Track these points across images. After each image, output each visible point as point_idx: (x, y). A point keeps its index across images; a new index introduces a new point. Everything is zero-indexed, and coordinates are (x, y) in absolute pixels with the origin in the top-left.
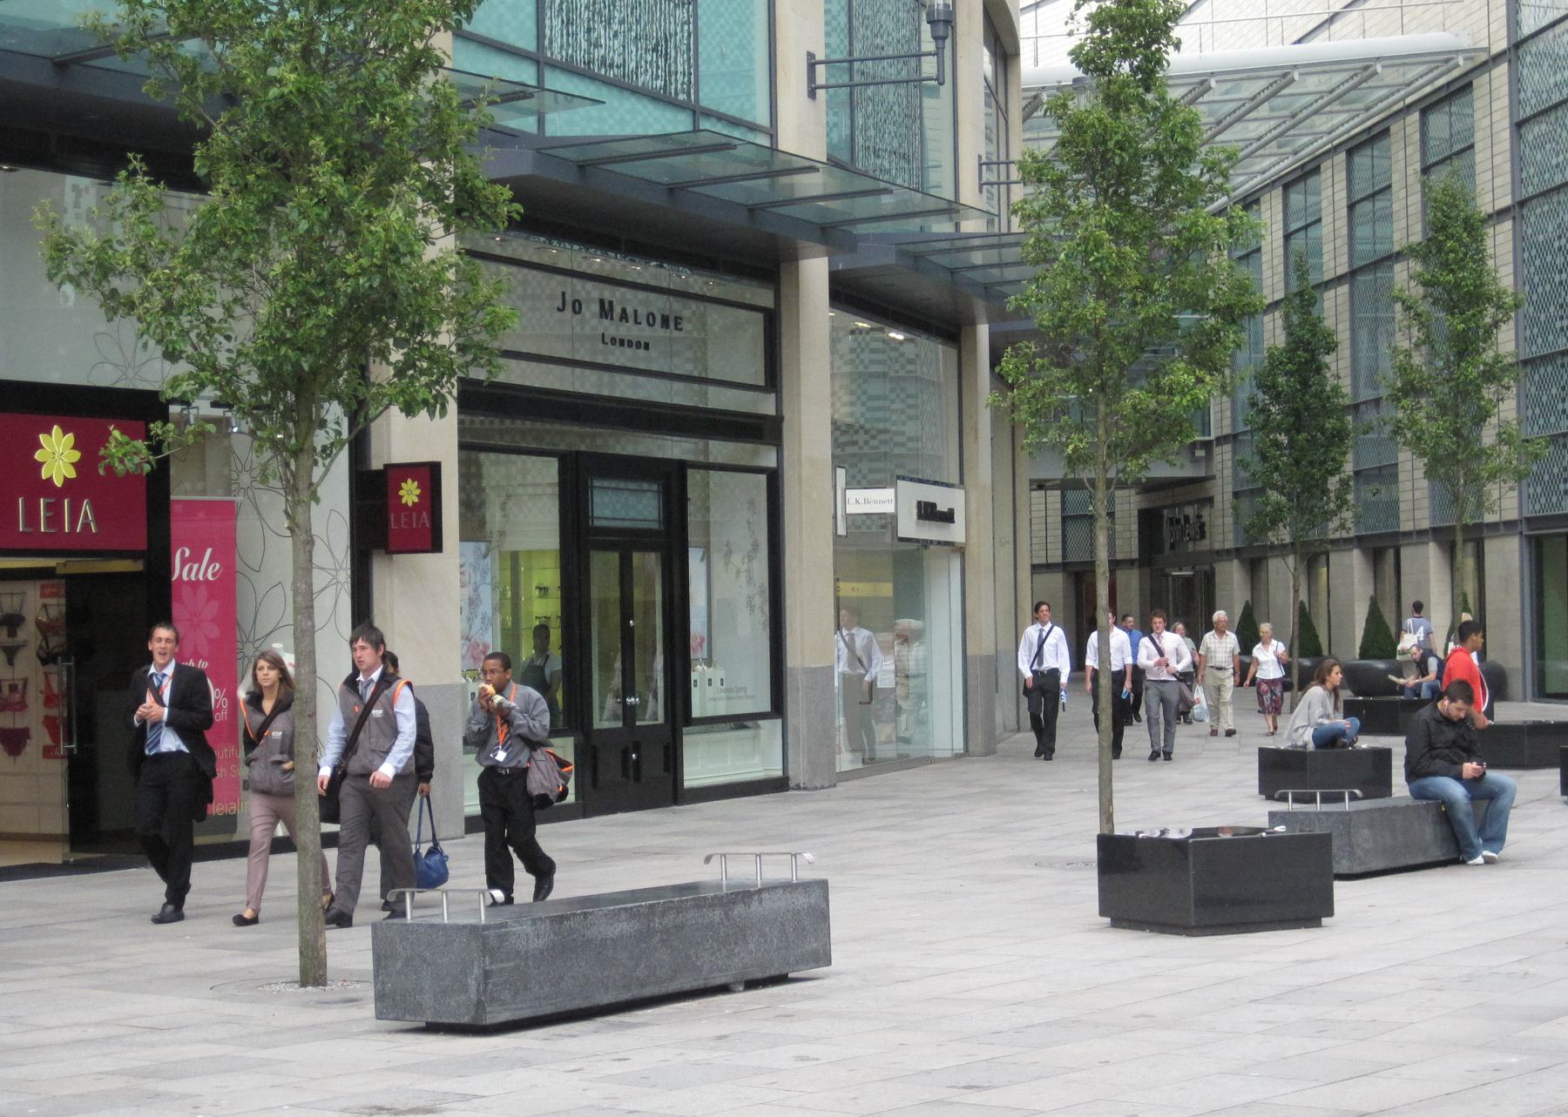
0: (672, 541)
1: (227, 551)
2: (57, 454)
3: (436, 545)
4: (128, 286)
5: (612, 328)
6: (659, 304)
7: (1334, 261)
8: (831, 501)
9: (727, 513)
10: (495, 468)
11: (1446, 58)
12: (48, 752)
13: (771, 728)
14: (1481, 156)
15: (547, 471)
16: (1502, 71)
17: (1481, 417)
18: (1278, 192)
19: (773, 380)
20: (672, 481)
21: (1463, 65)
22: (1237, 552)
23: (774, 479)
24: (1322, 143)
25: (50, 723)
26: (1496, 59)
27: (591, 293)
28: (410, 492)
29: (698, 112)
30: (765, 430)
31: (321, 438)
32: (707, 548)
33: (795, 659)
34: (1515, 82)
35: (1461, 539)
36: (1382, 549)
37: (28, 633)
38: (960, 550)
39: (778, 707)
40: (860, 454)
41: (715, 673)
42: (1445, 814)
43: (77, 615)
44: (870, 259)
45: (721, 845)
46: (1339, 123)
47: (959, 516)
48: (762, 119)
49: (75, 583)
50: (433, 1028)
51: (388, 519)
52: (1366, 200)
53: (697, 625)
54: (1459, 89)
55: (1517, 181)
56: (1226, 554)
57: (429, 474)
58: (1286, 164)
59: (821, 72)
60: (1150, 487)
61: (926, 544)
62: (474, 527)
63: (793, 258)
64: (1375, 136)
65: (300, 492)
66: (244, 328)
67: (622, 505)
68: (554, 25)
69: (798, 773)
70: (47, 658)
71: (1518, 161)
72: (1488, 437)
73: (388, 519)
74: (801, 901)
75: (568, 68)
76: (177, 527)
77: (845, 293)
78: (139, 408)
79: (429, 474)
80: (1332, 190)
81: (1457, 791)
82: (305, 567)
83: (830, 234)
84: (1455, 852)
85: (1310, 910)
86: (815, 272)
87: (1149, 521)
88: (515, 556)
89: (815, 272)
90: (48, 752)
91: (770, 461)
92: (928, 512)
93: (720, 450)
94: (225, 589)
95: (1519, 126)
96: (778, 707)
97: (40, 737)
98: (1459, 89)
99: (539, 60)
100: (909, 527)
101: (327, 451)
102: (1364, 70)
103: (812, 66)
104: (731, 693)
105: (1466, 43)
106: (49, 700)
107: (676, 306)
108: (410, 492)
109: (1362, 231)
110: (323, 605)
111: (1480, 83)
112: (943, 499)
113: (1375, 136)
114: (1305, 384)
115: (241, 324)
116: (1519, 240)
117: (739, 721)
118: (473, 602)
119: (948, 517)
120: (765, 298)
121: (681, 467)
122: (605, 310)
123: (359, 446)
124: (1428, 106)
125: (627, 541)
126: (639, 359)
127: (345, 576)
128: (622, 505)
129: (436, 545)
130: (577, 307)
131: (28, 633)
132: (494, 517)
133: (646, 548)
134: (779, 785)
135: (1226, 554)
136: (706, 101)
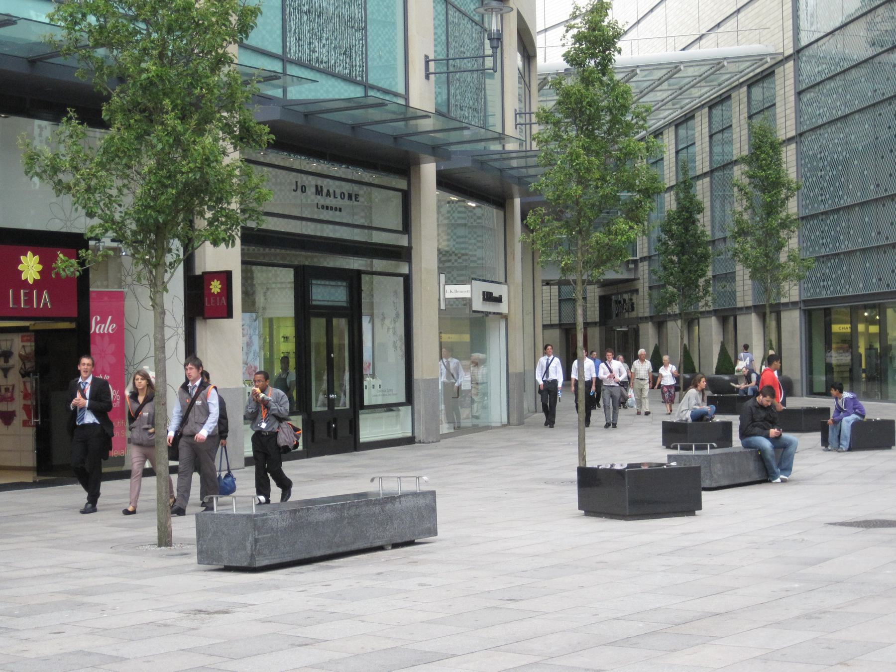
1: (119, 317)
2: (30, 267)
3: (229, 315)
4: (67, 178)
6: (347, 187)
7: (702, 165)
9: (383, 297)
10: (261, 274)
11: (761, 58)
13: (406, 411)
14: (779, 109)
15: (288, 275)
16: (790, 65)
19: (407, 227)
20: (353, 280)
21: (770, 62)
23: (408, 280)
24: (696, 103)
25: (26, 408)
26: (787, 58)
27: (311, 181)
28: (216, 287)
29: (367, 86)
30: (403, 254)
31: (169, 258)
34: (797, 71)
35: (769, 311)
36: (727, 317)
37: (15, 361)
38: (505, 317)
39: (410, 399)
40: (453, 266)
41: (377, 382)
42: (760, 456)
43: (40, 352)
44: (459, 164)
47: (505, 299)
48: (401, 90)
50: (228, 569)
54: (768, 75)
55: (798, 123)
58: (677, 114)
59: (432, 66)
60: (605, 284)
61: (487, 314)
62: (249, 305)
63: (417, 163)
64: (724, 99)
65: (158, 287)
66: (128, 200)
68: (292, 40)
69: (420, 435)
71: (799, 112)
73: (204, 301)
74: (421, 502)
76: (93, 305)
77: (445, 182)
79: (226, 277)
80: (701, 128)
81: (766, 444)
82: (160, 326)
83: (437, 151)
85: (688, 505)
86: (429, 171)
87: (604, 301)
88: (271, 320)
89: (429, 171)
90: (25, 424)
91: (405, 271)
92: (488, 297)
93: (379, 264)
94: (118, 338)
95: (799, 94)
97: (21, 416)
98: (768, 75)
99: (284, 59)
100: (478, 305)
102: (717, 64)
103: (427, 62)
105: (771, 50)
106: (26, 396)
107: (355, 188)
108: (216, 287)
109: (717, 149)
110: (170, 346)
111: (779, 71)
113: (724, 99)
114: (686, 229)
115: (127, 198)
117: (389, 407)
118: (249, 345)
119: (499, 300)
120: (402, 184)
121: (359, 273)
122: (319, 191)
124: (751, 84)
125: (330, 312)
127: (181, 331)
129: (229, 315)
130: (304, 189)
131: (15, 361)
132: (260, 299)
134: (410, 441)
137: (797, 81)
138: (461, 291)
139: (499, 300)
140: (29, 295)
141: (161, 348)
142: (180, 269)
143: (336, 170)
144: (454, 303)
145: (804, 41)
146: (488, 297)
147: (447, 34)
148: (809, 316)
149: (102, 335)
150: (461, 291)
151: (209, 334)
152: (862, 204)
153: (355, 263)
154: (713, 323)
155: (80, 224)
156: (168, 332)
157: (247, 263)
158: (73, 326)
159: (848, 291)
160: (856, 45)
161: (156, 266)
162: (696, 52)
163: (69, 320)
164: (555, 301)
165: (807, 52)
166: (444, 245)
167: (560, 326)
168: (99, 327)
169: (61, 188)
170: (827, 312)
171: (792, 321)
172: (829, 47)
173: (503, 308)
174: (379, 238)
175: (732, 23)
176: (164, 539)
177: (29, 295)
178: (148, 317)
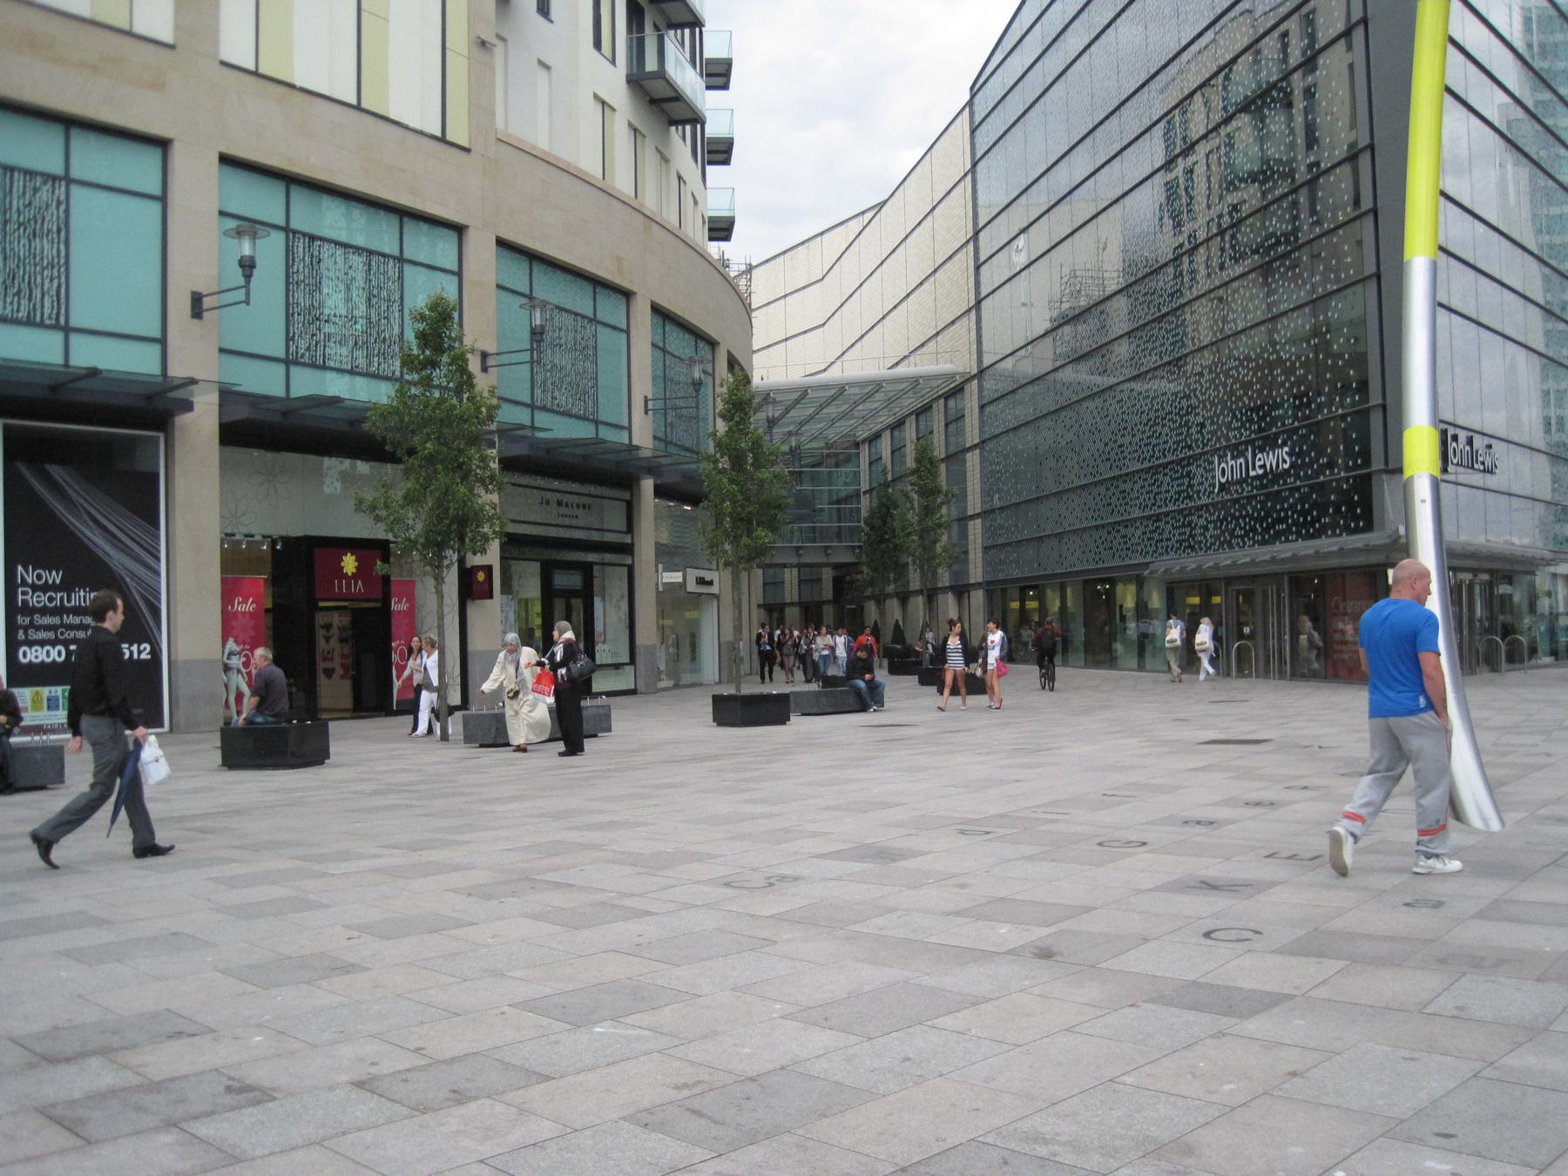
0: (587, 594)
1: (411, 599)
2: (349, 563)
3: (491, 597)
4: (383, 513)
5: (563, 510)
6: (583, 500)
7: (939, 452)
8: (657, 577)
9: (614, 583)
10: (517, 567)
11: (952, 376)
12: (342, 677)
13: (629, 669)
14: (967, 420)
15: (535, 567)
16: (975, 382)
17: (935, 542)
18: (888, 432)
19: (630, 528)
20: (586, 569)
21: (959, 380)
22: (951, 588)
23: (631, 569)
24: (906, 411)
25: (343, 665)
26: (973, 377)
27: (554, 497)
28: (481, 576)
29: (597, 422)
30: (628, 549)
31: (446, 562)
32: (604, 599)
33: (639, 641)
34: (980, 387)
35: (961, 591)
36: (904, 599)
37: (335, 631)
38: (716, 597)
39: (632, 661)
40: (668, 555)
41: (606, 647)
42: (858, 692)
43: (354, 624)
44: (671, 478)
45: (770, 816)
46: (910, 403)
47: (716, 583)
48: (626, 423)
49: (355, 612)
50: (482, 746)
51: (472, 588)
52: (955, 420)
53: (599, 627)
54: (958, 391)
55: (981, 432)
56: (945, 590)
57: (488, 569)
58: (891, 420)
59: (650, 405)
60: (836, 566)
61: (700, 594)
62: (507, 587)
63: (638, 480)
64: (927, 408)
65: (439, 580)
66: (419, 527)
67: (562, 580)
68: (538, 392)
69: (641, 687)
70: (343, 640)
71: (982, 424)
72: (939, 549)
73: (472, 588)
74: (601, 711)
75: (544, 409)
76: (393, 589)
77: (660, 492)
78: (380, 548)
79: (488, 569)
80: (937, 420)
81: (862, 684)
82: (441, 604)
83: (651, 469)
84: (863, 708)
85: (782, 720)
86: (648, 485)
87: (838, 582)
88: (526, 601)
89: (648, 485)
90: (342, 677)
91: (629, 561)
92: (701, 581)
93: (608, 557)
94: (411, 614)
95: (982, 407)
96: (632, 661)
97: (339, 671)
98: (958, 391)
99: (532, 406)
100: (692, 587)
101: (448, 567)
102: (915, 382)
103: (646, 401)
104: (615, 654)
105: (961, 370)
106: (343, 656)
107: (589, 500)
108: (481, 576)
109: (952, 439)
110: (447, 621)
111: (967, 387)
112: (708, 576)
113: (927, 408)
114: (885, 522)
115: (416, 524)
116: (983, 459)
117: (617, 666)
118: (506, 618)
119: (710, 583)
120: (627, 496)
121: (591, 564)
122: (559, 503)
123: (461, 561)
124: (948, 396)
125: (568, 594)
126: (574, 522)
127: (456, 608)
128: (562, 580)
129: (491, 597)
130: (548, 503)
131: (335, 631)
132: (515, 586)
133: (576, 596)
134: (633, 692)
135: (945, 590)
136: (602, 417)
137: (980, 397)
138: (676, 577)
139: (710, 583)
140: (348, 585)
141: (441, 617)
142: (455, 567)
143: (575, 487)
144: (671, 586)
145: (987, 362)
146: (701, 581)
147: (663, 379)
148: (990, 595)
149: (244, 613)
150: (676, 577)
151: (476, 610)
152: (1026, 502)
153: (591, 557)
154: (950, 598)
155: (379, 532)
156: (446, 610)
157: (503, 559)
158: (321, 604)
159: (1016, 574)
160: (1042, 360)
161: (437, 567)
162: (902, 370)
163: (375, 600)
164: (796, 581)
165: (989, 372)
166: (665, 538)
167: (800, 604)
168: (397, 606)
169: (378, 519)
170: (1004, 591)
171: (978, 597)
172: (1008, 364)
173: (715, 589)
174: (610, 537)
175: (932, 344)
176: (445, 737)
177: (348, 585)
178: (432, 599)
